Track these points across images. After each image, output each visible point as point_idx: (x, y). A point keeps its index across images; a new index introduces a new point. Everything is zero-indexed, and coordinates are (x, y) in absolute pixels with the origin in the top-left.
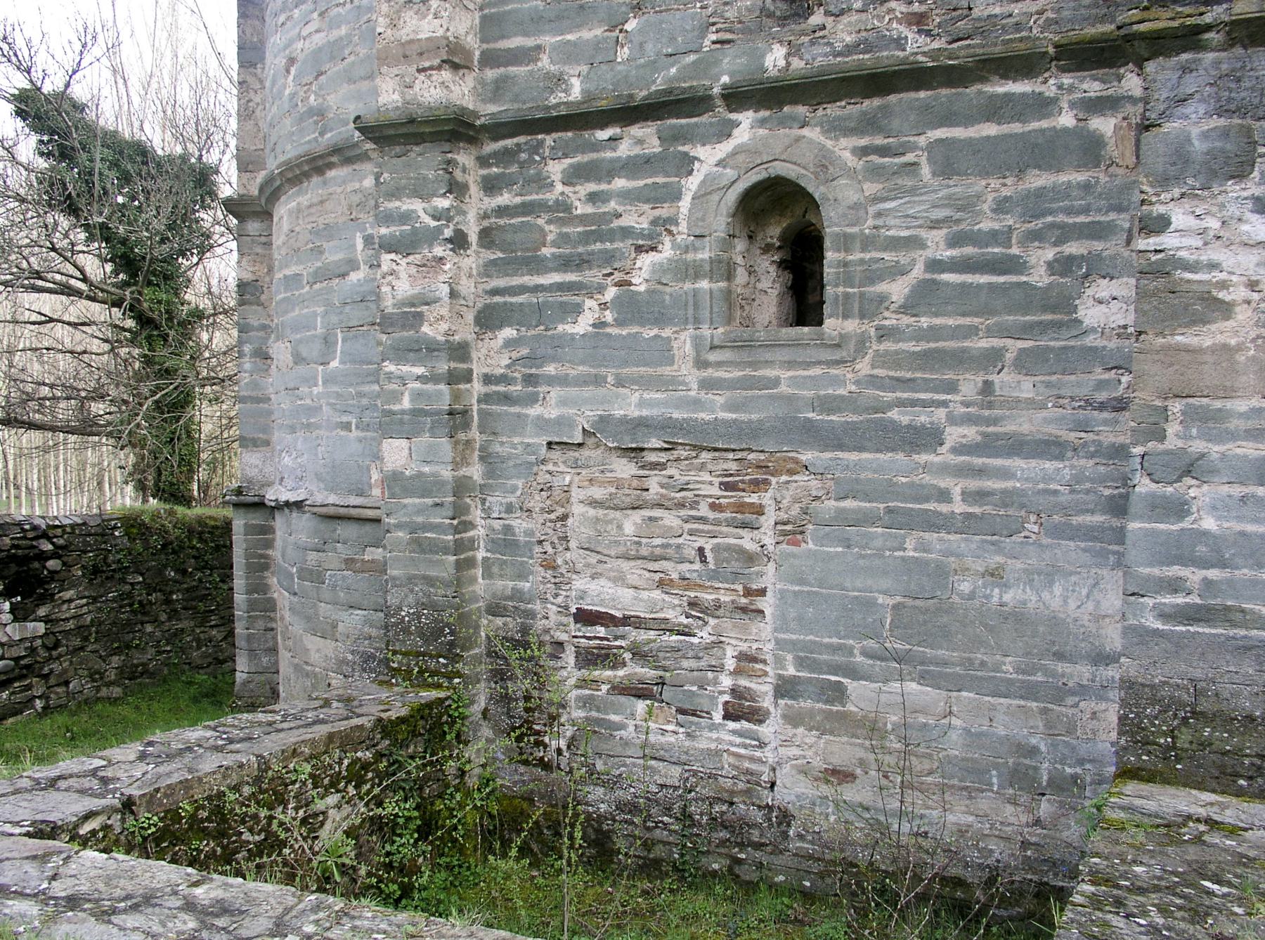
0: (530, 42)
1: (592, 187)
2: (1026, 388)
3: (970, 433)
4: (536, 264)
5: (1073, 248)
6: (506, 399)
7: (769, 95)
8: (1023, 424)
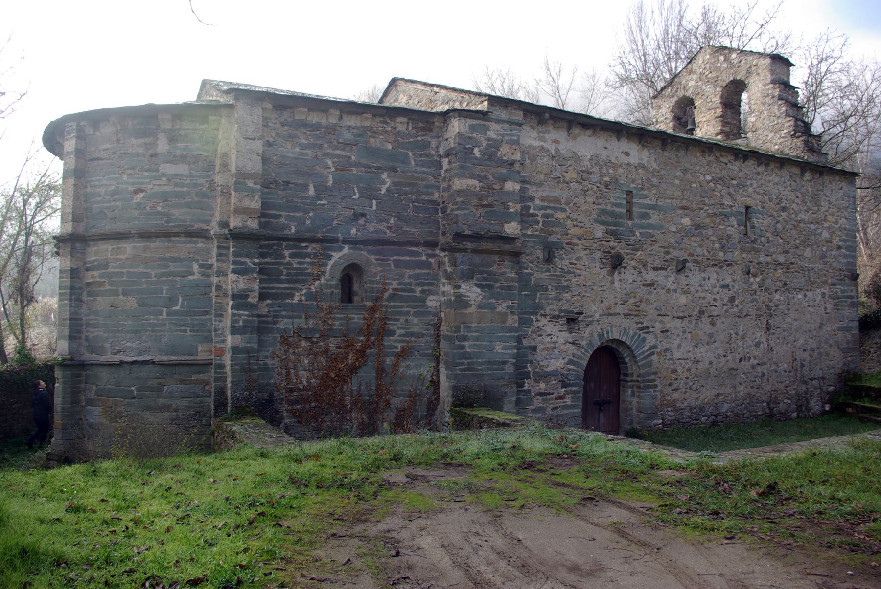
0: (278, 213)
1: (299, 260)
2: (415, 321)
3: (403, 332)
4: (281, 282)
5: (426, 288)
6: (267, 322)
7: (354, 242)
8: (415, 329)
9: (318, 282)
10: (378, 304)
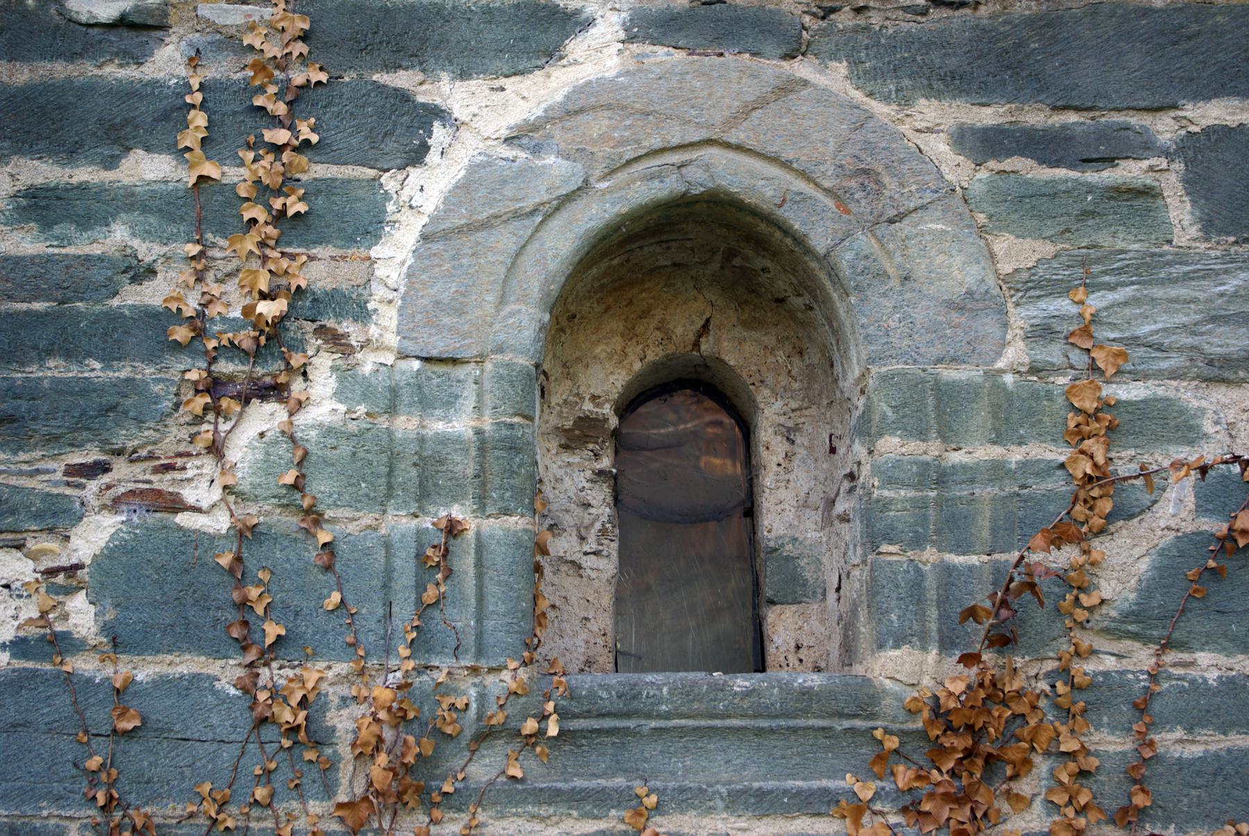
1: (41, 172)
9: (265, 417)
10: (1030, 672)
